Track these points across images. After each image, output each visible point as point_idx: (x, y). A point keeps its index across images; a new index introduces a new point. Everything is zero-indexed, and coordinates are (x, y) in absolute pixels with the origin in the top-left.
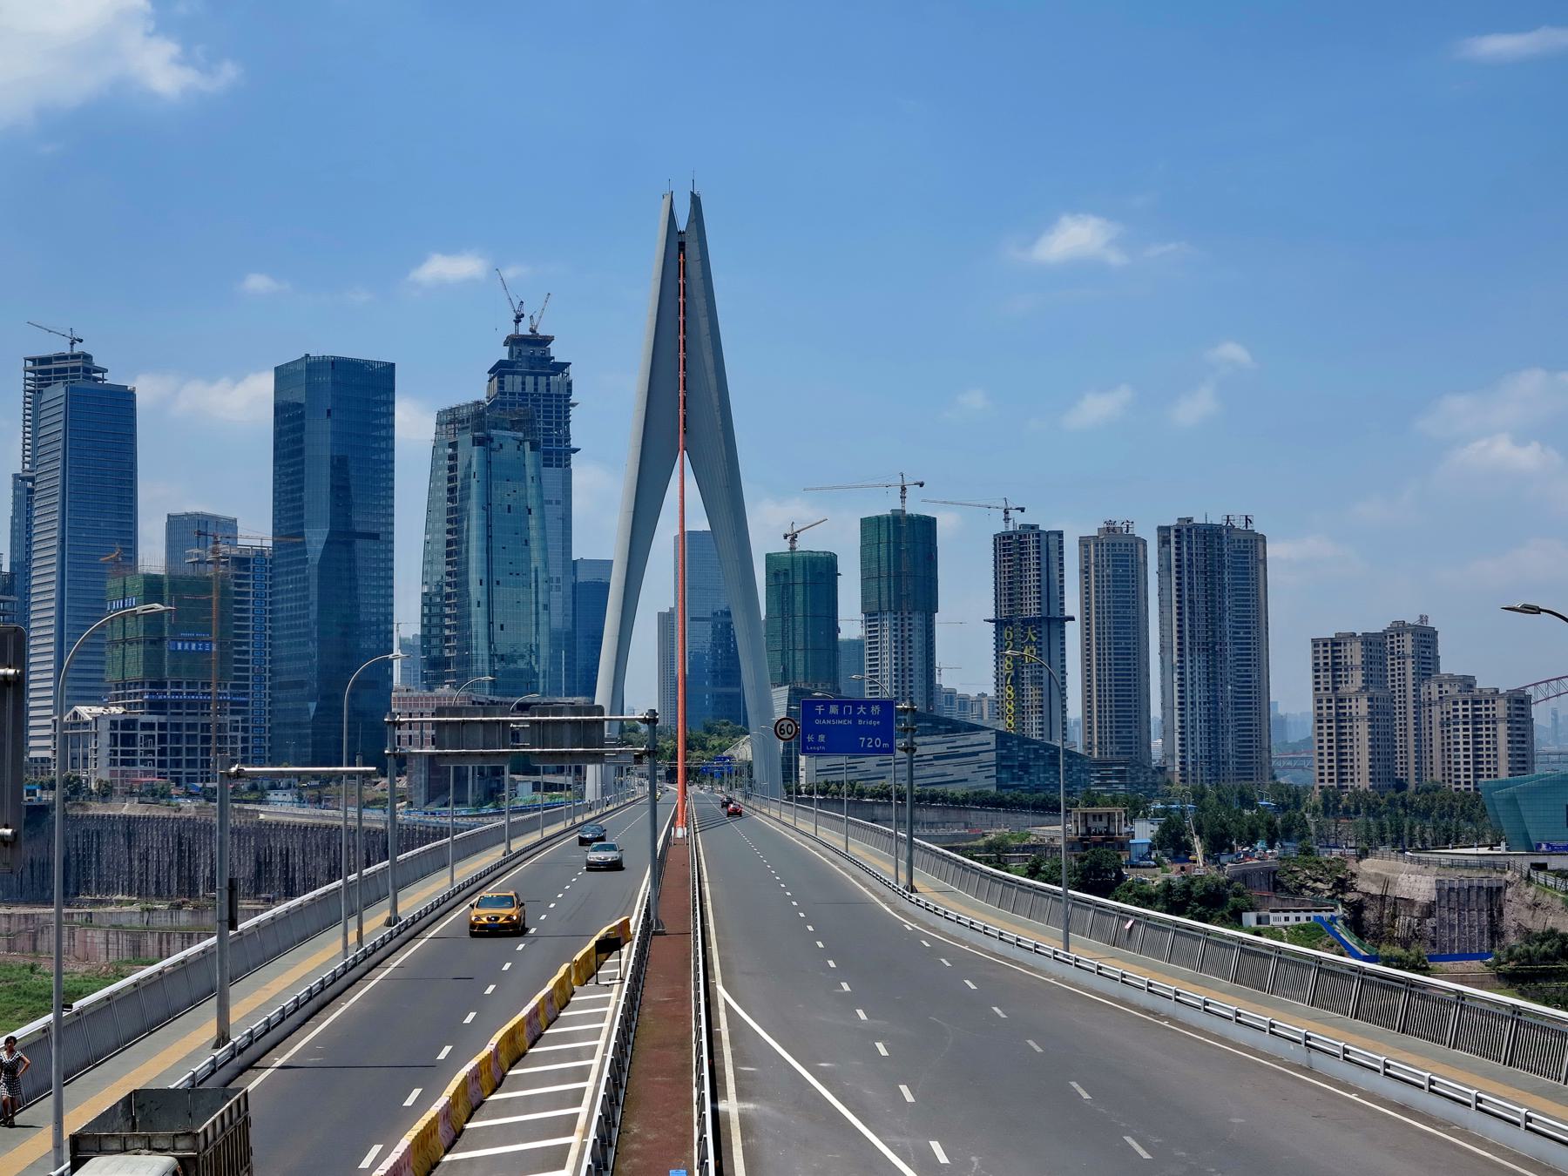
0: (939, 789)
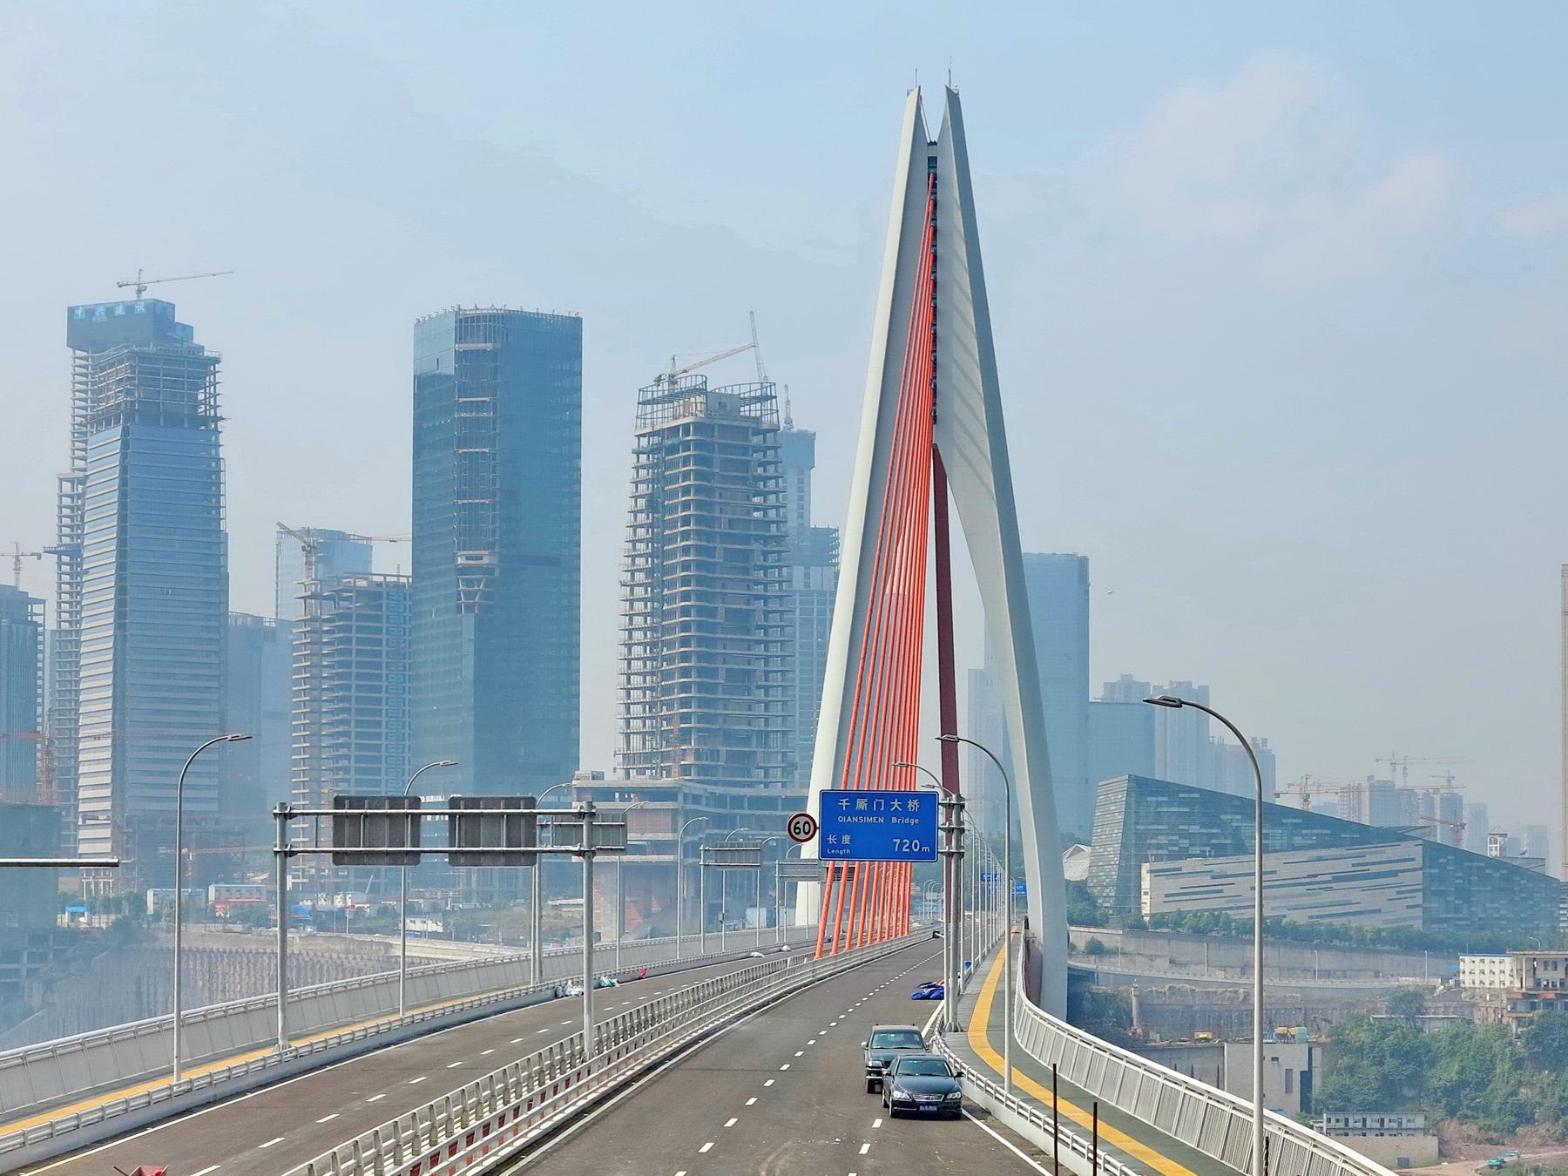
0: (1337, 922)
